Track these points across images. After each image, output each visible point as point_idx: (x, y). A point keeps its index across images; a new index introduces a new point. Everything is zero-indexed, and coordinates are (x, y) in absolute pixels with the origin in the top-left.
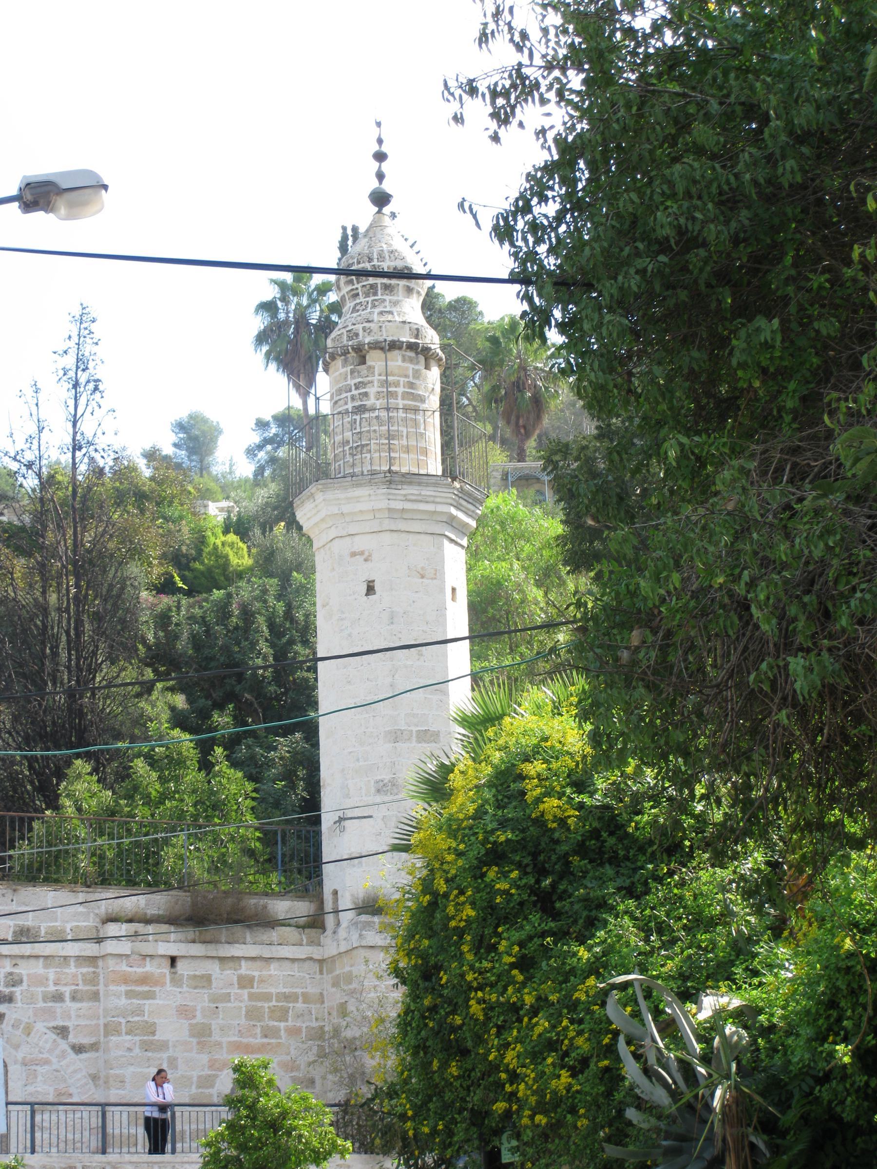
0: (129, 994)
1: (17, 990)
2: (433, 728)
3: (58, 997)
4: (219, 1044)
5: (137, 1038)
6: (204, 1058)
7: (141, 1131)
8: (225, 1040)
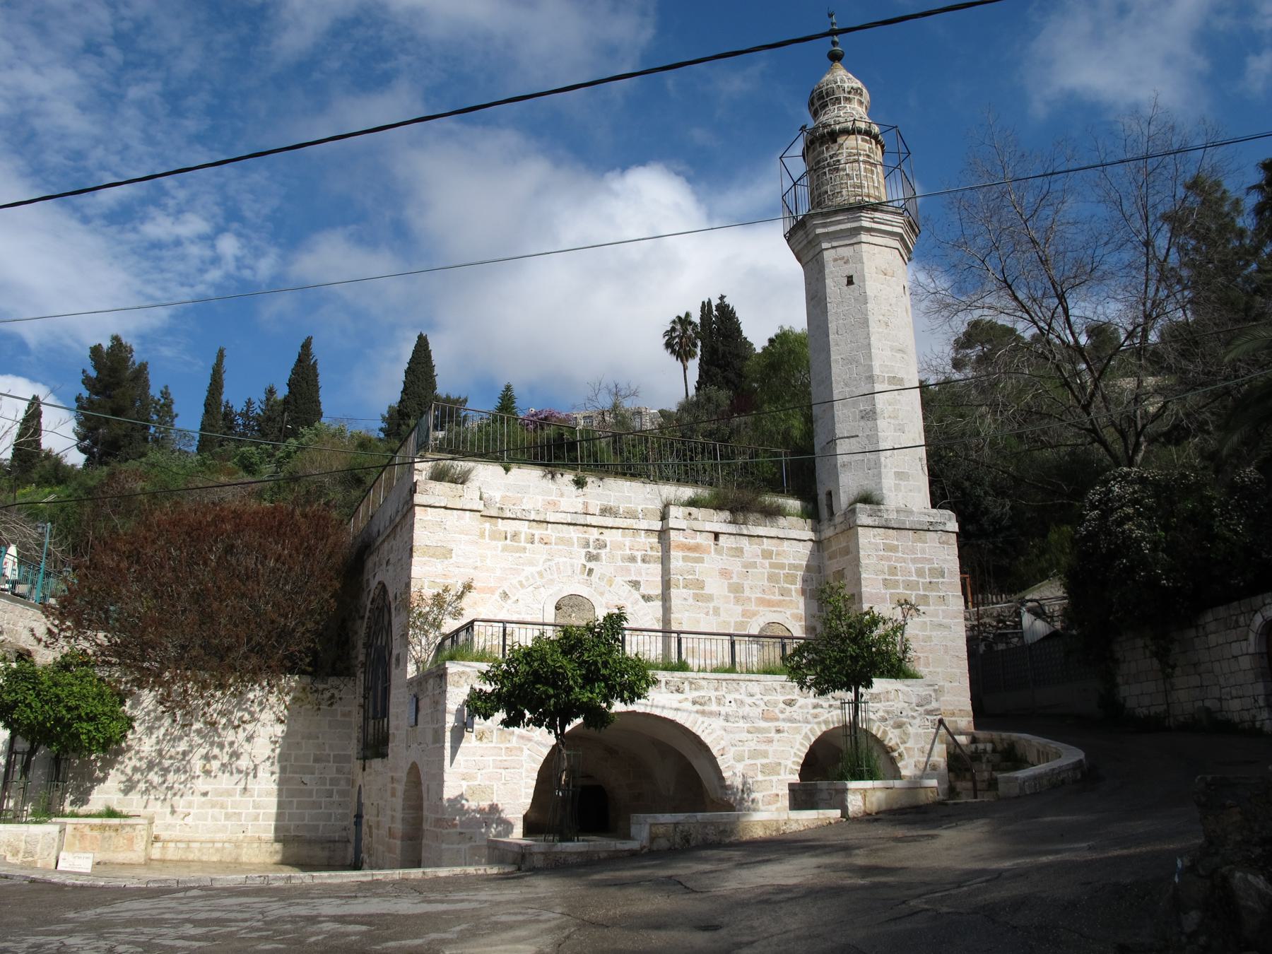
0: (685, 559)
1: (603, 552)
2: (899, 376)
3: (632, 559)
4: (749, 599)
6: (739, 609)
8: (753, 596)
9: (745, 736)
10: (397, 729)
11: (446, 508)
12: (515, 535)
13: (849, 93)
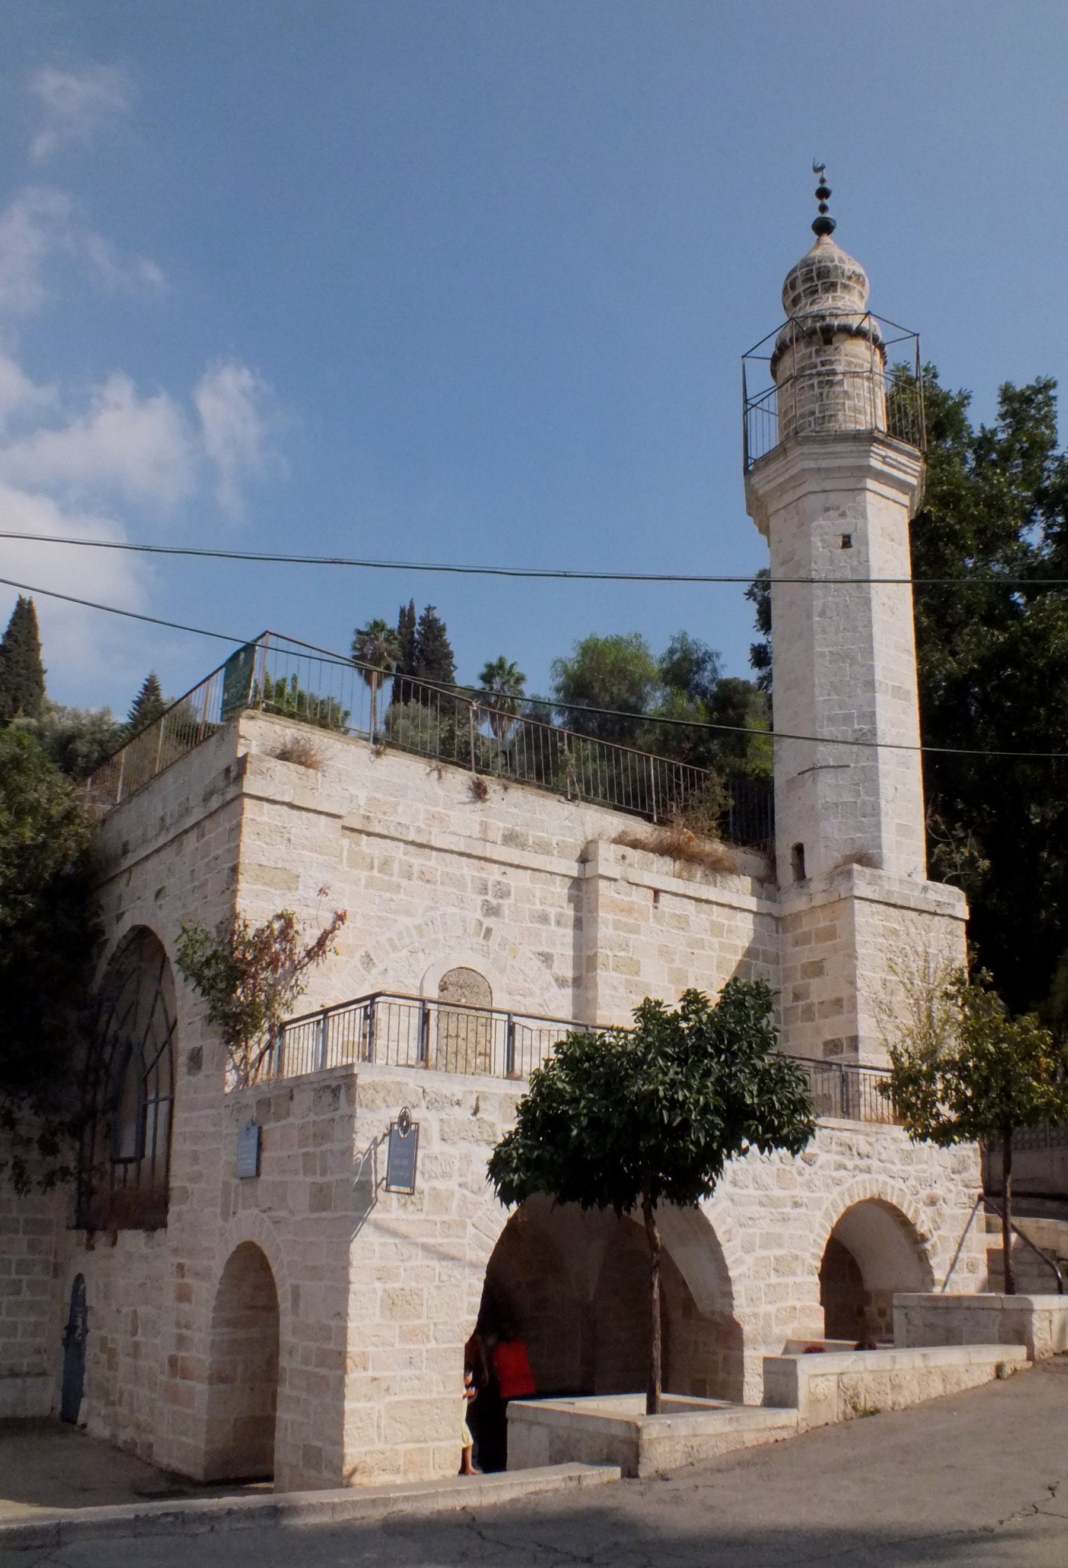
0: (617, 925)
1: (506, 903)
3: (544, 919)
5: (624, 977)
7: (984, 1257)
9: (755, 1210)
10: (195, 1178)
11: (291, 806)
12: (385, 864)
13: (850, 278)
